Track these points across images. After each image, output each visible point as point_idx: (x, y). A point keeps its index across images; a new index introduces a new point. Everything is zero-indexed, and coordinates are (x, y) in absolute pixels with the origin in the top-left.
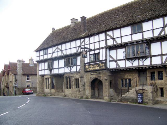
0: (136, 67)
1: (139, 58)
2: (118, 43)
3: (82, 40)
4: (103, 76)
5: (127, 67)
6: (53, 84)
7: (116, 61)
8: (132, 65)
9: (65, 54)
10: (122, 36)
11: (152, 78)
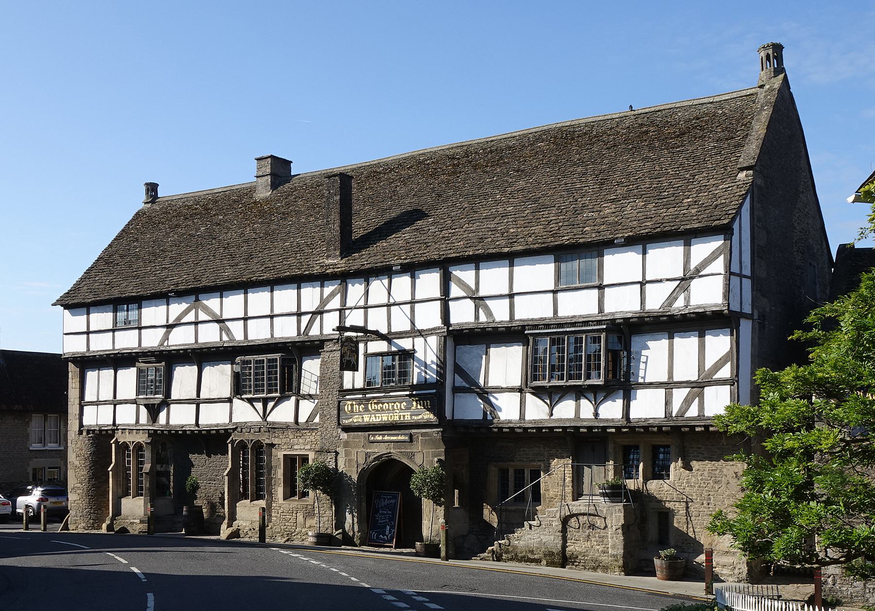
2: (498, 319)
5: (530, 422)
9: (239, 336)
10: (515, 291)
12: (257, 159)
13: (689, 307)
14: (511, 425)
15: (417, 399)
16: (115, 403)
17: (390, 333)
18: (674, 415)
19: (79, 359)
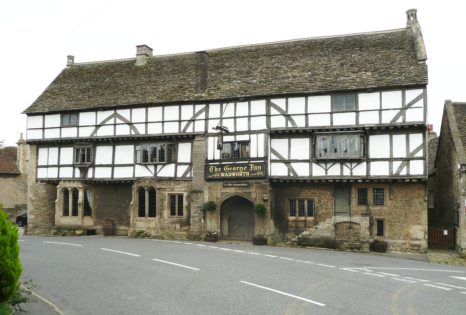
0: (336, 178)
1: (342, 162)
2: (298, 126)
3: (199, 107)
4: (258, 191)
5: (315, 177)
6: (88, 204)
7: (287, 162)
8: (326, 173)
11: (363, 201)
12: (137, 46)
13: (405, 123)
14: (304, 179)
15: (253, 165)
16: (59, 166)
17: (235, 131)
18: (394, 174)
19: (59, 141)
